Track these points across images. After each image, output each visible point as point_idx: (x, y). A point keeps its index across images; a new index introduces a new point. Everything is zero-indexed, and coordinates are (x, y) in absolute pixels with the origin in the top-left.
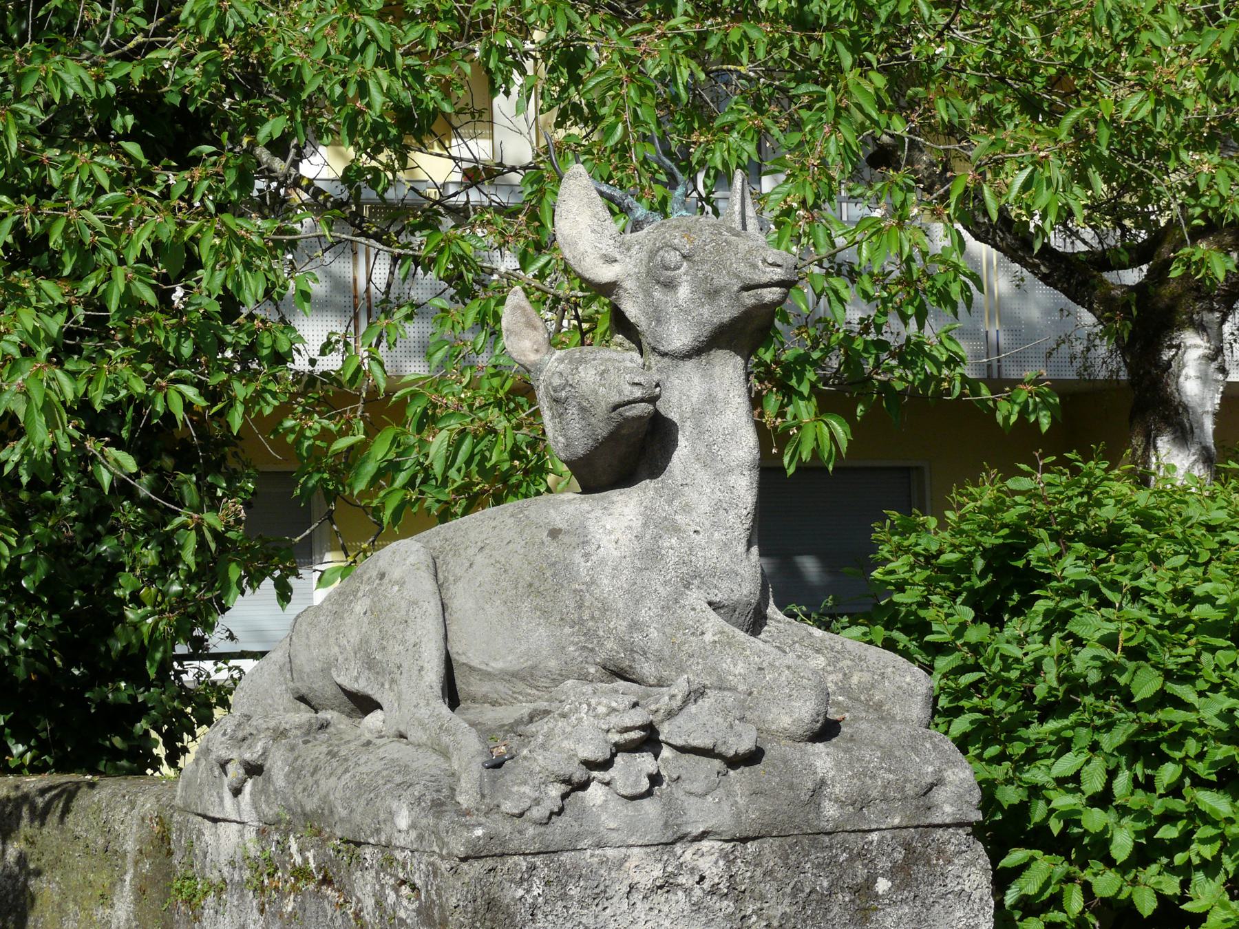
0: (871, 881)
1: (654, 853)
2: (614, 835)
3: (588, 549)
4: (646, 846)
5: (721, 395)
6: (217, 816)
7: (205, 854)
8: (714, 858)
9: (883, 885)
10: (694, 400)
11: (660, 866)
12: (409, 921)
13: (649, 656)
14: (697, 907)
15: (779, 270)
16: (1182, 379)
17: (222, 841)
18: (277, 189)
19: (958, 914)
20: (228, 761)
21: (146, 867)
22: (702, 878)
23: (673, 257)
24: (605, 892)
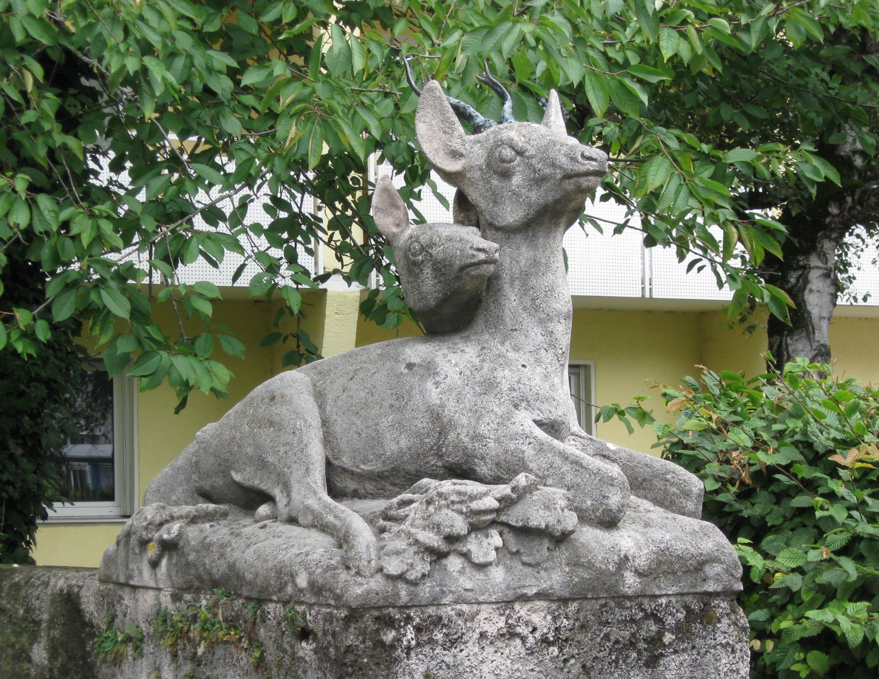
0: (660, 634)
1: (498, 609)
2: (470, 594)
3: (437, 379)
4: (497, 603)
5: (543, 261)
6: (137, 584)
7: (125, 615)
8: (543, 614)
9: (668, 638)
10: (522, 264)
11: (503, 618)
12: (307, 659)
13: (487, 460)
14: (531, 652)
15: (594, 163)
16: (807, 292)
17: (140, 603)
18: (176, 109)
19: (724, 661)
20: (149, 541)
21: (56, 633)
22: (535, 629)
23: (508, 153)
24: (462, 638)
